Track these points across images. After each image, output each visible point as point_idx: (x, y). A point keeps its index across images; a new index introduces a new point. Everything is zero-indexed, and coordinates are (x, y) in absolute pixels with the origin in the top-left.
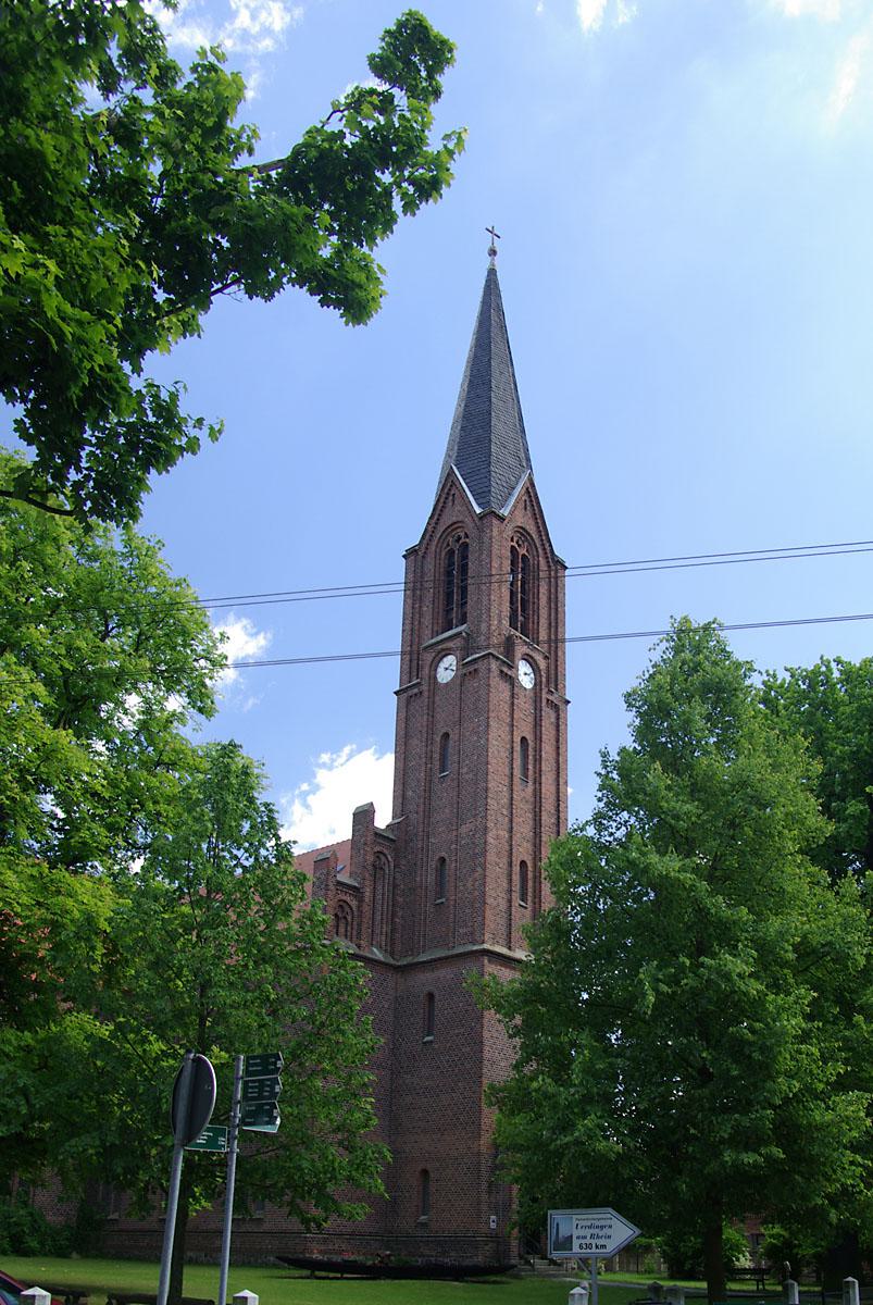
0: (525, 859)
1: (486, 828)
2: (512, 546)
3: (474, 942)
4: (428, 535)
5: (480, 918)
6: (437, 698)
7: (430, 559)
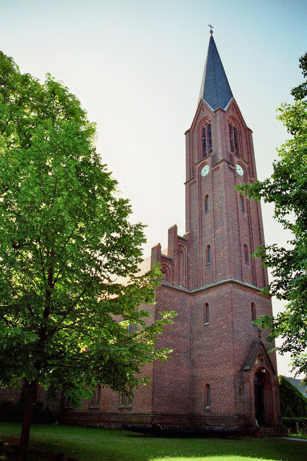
0: (246, 243)
6: (202, 182)
7: (195, 132)
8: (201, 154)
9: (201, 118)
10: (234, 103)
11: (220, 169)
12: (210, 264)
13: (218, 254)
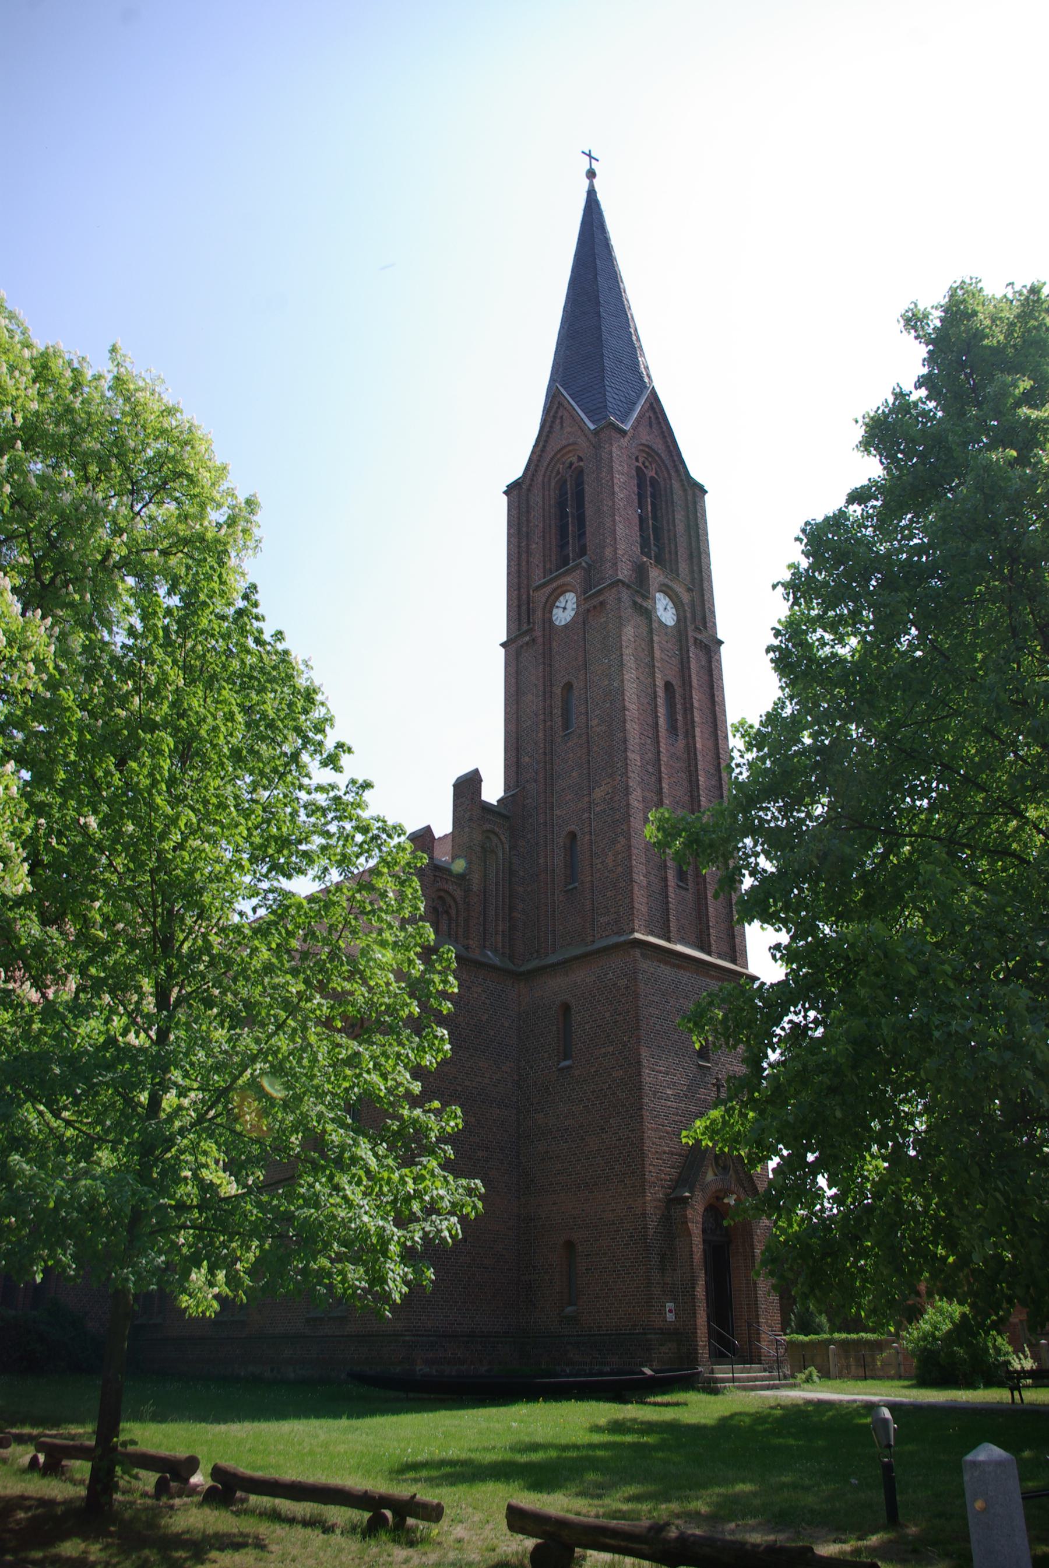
1: (627, 788)
2: (637, 467)
3: (619, 933)
4: (524, 473)
5: (627, 901)
8: (554, 558)
9: (554, 445)
10: (655, 405)
11: (608, 606)
12: (576, 888)
13: (598, 861)
